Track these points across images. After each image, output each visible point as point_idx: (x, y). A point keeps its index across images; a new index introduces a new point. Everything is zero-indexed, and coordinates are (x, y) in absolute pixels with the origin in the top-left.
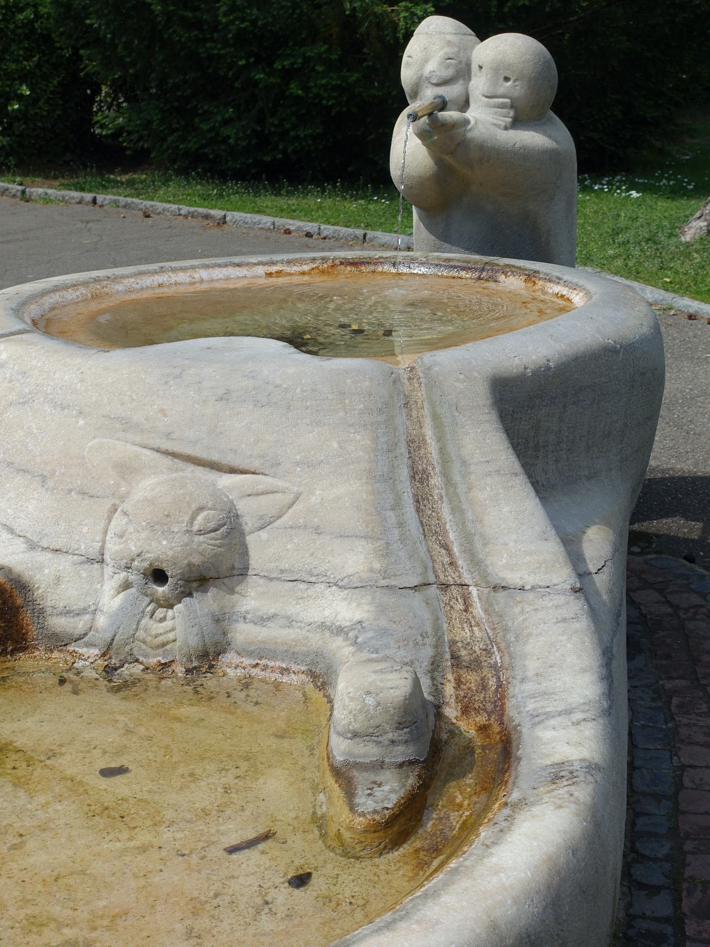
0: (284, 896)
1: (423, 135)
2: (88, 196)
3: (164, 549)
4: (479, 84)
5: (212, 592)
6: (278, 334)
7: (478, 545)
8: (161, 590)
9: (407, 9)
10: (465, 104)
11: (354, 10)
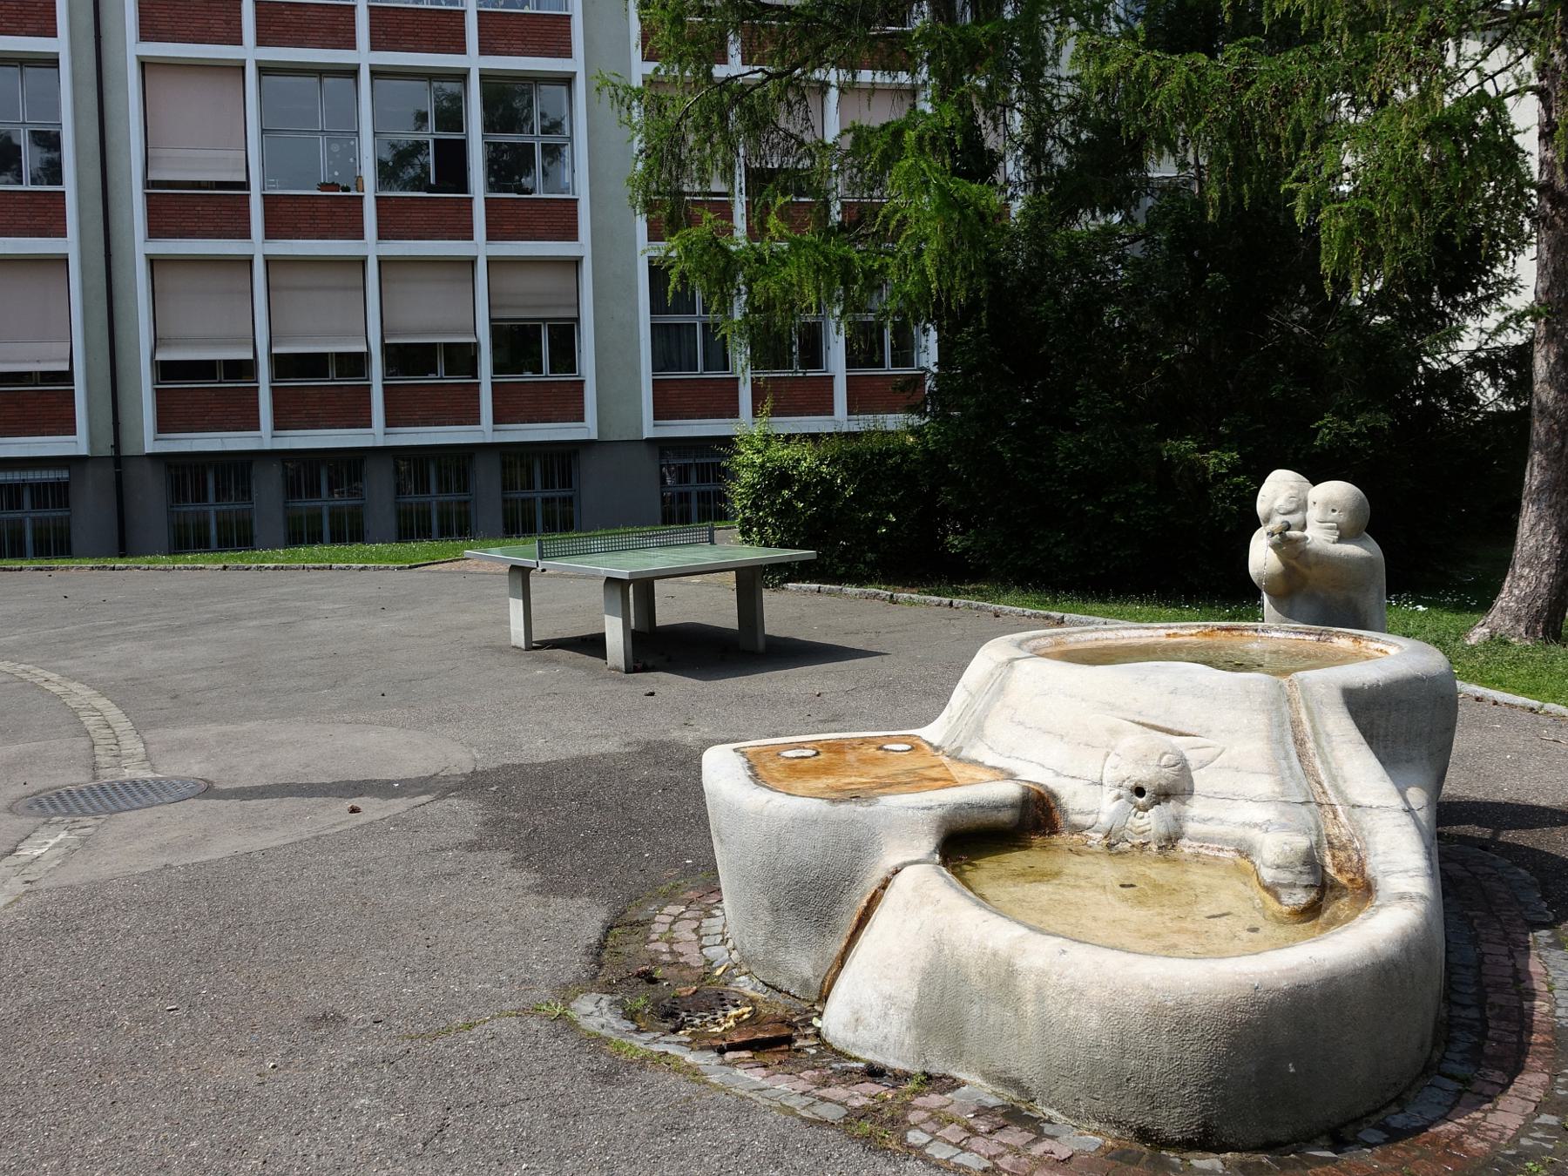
0: (1245, 935)
1: (1275, 546)
2: (946, 600)
3: (1145, 774)
4: (1313, 514)
5: (1172, 802)
6: (1202, 657)
7: (1340, 782)
8: (1141, 800)
9: (1216, 456)
10: (1304, 527)
11: (1170, 457)
